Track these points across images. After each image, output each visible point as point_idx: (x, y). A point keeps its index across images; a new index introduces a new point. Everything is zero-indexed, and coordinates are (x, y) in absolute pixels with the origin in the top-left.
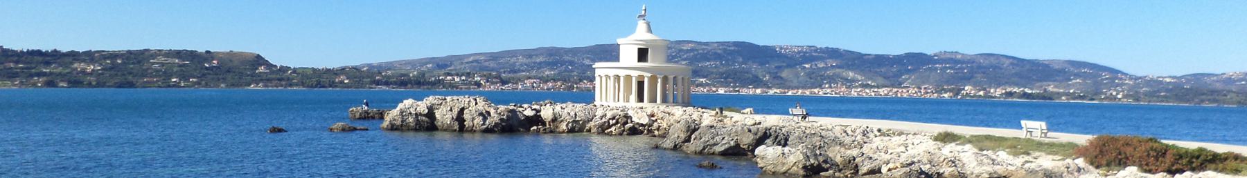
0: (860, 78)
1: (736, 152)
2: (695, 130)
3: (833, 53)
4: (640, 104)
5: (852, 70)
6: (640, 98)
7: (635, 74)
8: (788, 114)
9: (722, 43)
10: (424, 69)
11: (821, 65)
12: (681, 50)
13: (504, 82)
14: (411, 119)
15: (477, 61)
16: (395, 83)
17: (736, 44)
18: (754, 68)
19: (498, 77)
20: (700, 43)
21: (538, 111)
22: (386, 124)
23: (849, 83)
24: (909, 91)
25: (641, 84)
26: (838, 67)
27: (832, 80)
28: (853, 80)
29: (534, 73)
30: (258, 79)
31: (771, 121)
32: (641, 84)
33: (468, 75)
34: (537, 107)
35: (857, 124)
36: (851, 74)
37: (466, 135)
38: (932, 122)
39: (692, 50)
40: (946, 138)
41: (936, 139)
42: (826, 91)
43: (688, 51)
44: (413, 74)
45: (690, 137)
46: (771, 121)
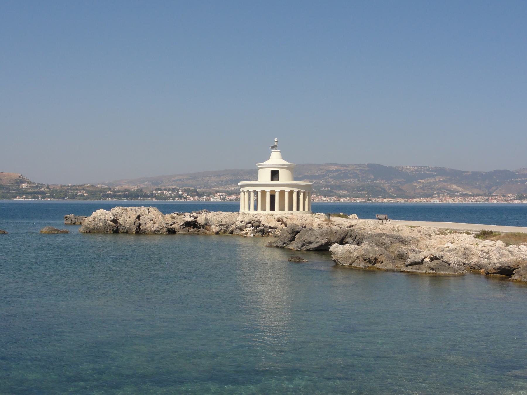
0: (460, 189)
1: (323, 250)
2: (298, 232)
3: (441, 171)
4: (272, 212)
5: (454, 184)
6: (273, 208)
7: (287, 189)
8: (348, 218)
9: (359, 165)
10: (142, 186)
11: (432, 180)
12: (330, 171)
13: (200, 195)
14: (101, 224)
15: (180, 180)
16: (121, 196)
17: (369, 165)
18: (384, 183)
19: (195, 191)
20: (343, 166)
21: (195, 218)
22: (81, 229)
23: (453, 194)
24: (497, 200)
25: (273, 197)
26: (444, 181)
27: (440, 192)
28: (456, 191)
29: (221, 188)
30: (22, 192)
31: (341, 222)
32: (273, 197)
33: (174, 190)
34: (195, 215)
35: (425, 226)
36: (454, 187)
37: (142, 237)
38: (469, 222)
39: (337, 171)
40: (485, 235)
41: (477, 236)
42: (436, 200)
43: (334, 171)
44: (134, 188)
45: (294, 237)
46: (341, 222)
